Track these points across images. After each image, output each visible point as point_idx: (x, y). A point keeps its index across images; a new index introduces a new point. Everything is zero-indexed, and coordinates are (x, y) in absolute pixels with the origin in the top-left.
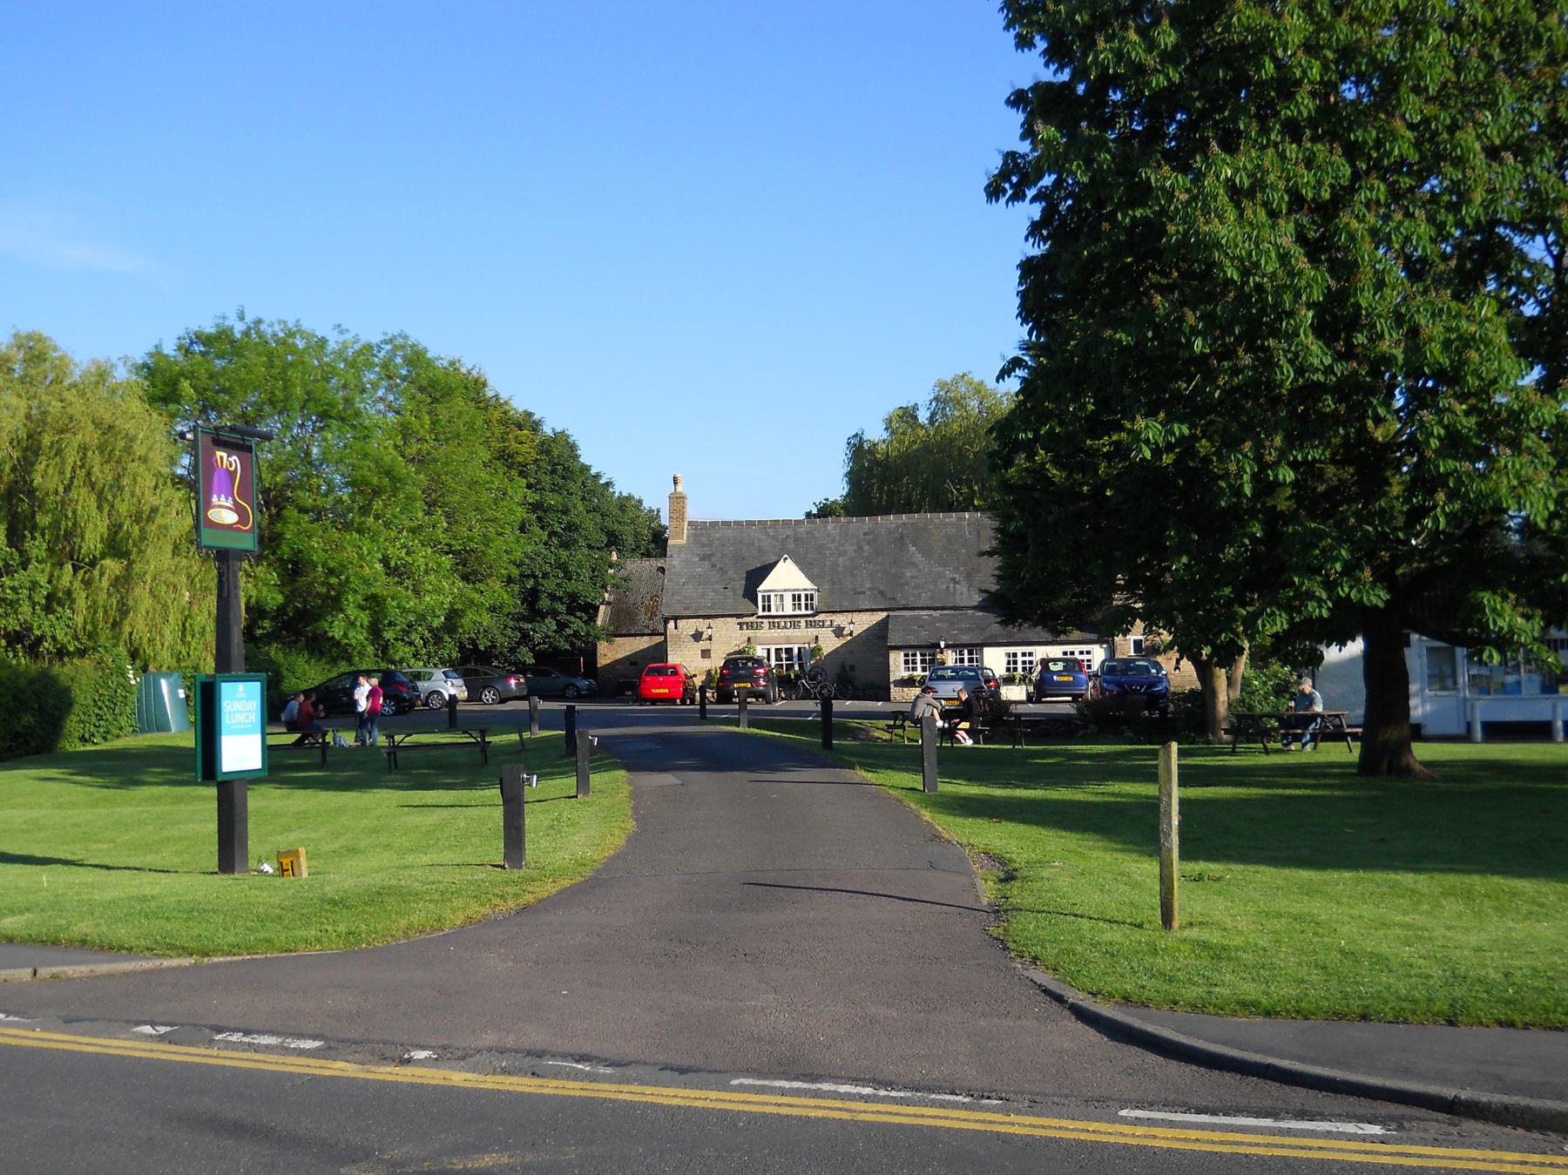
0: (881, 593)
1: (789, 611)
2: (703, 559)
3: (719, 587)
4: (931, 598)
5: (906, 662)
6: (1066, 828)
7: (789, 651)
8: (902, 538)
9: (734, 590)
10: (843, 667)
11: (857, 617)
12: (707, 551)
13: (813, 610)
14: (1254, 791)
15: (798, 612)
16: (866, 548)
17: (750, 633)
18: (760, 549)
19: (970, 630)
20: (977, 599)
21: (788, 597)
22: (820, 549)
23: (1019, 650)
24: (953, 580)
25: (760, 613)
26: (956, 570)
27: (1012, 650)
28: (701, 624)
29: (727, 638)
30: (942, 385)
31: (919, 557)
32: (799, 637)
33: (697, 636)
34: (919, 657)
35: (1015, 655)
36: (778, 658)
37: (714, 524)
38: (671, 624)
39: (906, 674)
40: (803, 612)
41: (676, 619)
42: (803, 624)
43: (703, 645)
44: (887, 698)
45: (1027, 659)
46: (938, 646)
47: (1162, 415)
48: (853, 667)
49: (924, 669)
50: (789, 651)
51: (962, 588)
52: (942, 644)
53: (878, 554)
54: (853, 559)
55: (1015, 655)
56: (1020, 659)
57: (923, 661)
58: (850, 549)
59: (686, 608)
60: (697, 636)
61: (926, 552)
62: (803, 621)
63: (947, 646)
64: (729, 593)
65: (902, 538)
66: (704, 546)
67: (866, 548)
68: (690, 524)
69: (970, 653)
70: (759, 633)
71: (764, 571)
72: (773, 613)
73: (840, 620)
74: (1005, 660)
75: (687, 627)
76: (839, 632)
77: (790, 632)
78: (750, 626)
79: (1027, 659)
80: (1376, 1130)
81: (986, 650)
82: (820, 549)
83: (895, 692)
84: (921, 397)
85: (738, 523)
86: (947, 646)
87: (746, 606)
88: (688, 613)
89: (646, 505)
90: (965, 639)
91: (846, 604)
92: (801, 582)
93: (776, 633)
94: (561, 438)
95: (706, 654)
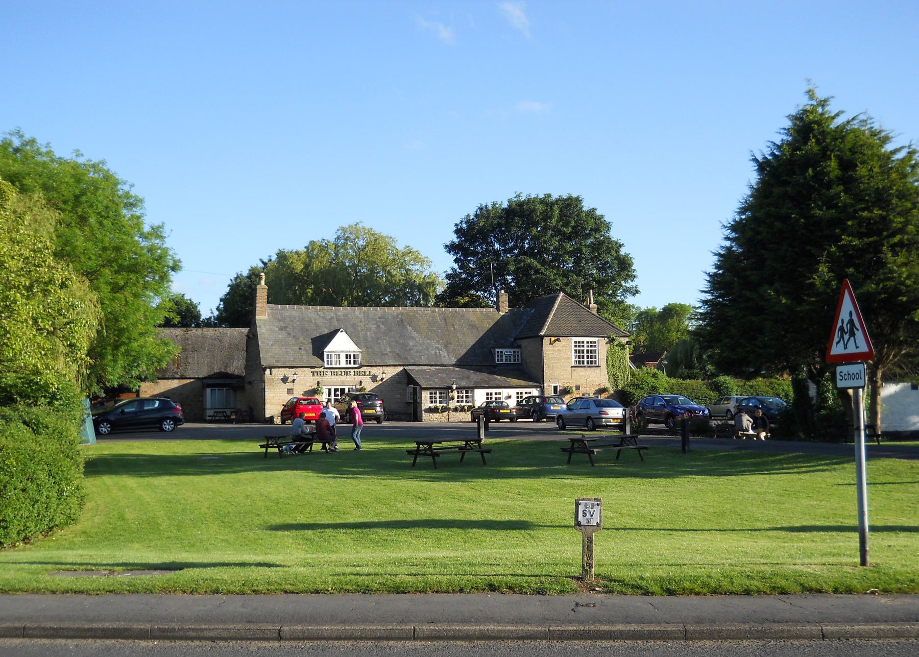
0: (398, 354)
1: (343, 364)
2: (281, 329)
3: (296, 348)
4: (428, 358)
5: (431, 398)
8: (402, 322)
9: (306, 350)
11: (386, 369)
12: (282, 324)
13: (354, 364)
14: (507, 469)
15: (349, 366)
16: (382, 326)
17: (319, 378)
20: (453, 361)
21: (343, 356)
23: (493, 391)
24: (437, 348)
25: (326, 366)
26: (438, 342)
27: (489, 391)
28: (289, 373)
29: (304, 381)
30: (344, 230)
31: (414, 334)
33: (285, 380)
34: (438, 395)
35: (491, 394)
40: (352, 365)
41: (271, 368)
42: (352, 373)
43: (289, 385)
44: (416, 417)
45: (498, 396)
46: (451, 388)
49: (441, 402)
51: (444, 353)
52: (454, 387)
53: (390, 331)
54: (376, 333)
55: (491, 394)
56: (494, 396)
57: (440, 397)
58: (373, 327)
59: (277, 361)
60: (285, 380)
61: (419, 331)
62: (352, 371)
64: (303, 352)
67: (382, 326)
69: (467, 392)
70: (325, 378)
72: (334, 366)
73: (375, 371)
74: (485, 396)
75: (279, 373)
76: (374, 378)
77: (344, 378)
78: (319, 374)
79: (498, 396)
81: (476, 391)
83: (425, 416)
84: (328, 234)
87: (315, 361)
88: (279, 364)
90: (463, 384)
91: (379, 362)
93: (335, 378)
95: (290, 391)
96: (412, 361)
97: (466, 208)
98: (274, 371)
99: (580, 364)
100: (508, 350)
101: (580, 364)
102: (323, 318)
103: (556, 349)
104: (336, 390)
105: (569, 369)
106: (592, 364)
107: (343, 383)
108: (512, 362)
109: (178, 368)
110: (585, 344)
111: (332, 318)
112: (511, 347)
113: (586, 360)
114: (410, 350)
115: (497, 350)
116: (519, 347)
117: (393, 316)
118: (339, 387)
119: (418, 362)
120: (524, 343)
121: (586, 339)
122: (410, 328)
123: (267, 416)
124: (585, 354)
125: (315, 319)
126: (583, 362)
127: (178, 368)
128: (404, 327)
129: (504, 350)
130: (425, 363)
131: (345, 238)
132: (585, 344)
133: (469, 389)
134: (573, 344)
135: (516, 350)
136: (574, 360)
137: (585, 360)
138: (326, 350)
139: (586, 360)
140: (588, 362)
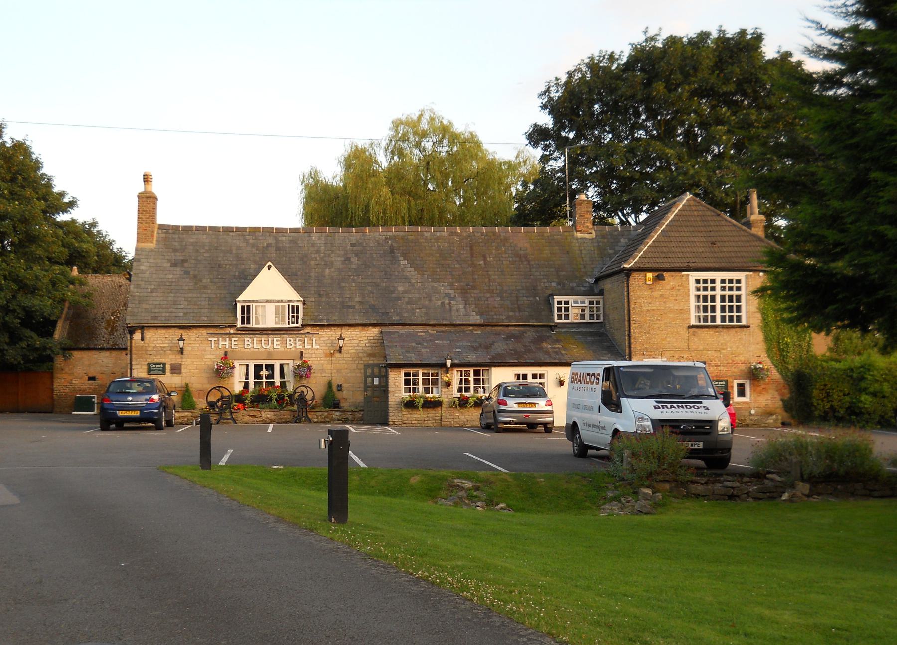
2: (174, 265)
4: (426, 313)
5: (407, 382)
6: (201, 438)
7: (270, 367)
10: (330, 384)
11: (347, 333)
12: (179, 256)
18: (239, 258)
19: (475, 349)
22: (304, 259)
23: (529, 371)
24: (447, 295)
26: (451, 285)
27: (522, 370)
31: (410, 271)
32: (283, 352)
36: (257, 376)
37: (188, 229)
38: (137, 336)
39: (406, 396)
41: (142, 328)
47: (870, 25)
48: (340, 388)
50: (270, 367)
51: (458, 304)
54: (340, 271)
58: (338, 261)
59: (155, 318)
61: (419, 268)
63: (454, 365)
65: (392, 251)
66: (175, 250)
67: (354, 259)
68: (161, 227)
71: (245, 279)
80: (120, 413)
82: (304, 259)
85: (212, 229)
86: (454, 365)
88: (156, 323)
89: (115, 247)
90: (472, 357)
91: (335, 318)
92: (288, 293)
94: (21, 147)
96: (395, 318)
97: (565, 59)
98: (149, 334)
99: (706, 325)
100: (579, 298)
101: (706, 325)
102: (253, 245)
103: (656, 294)
104: (258, 368)
105: (684, 333)
106: (732, 323)
107: (270, 355)
108: (587, 319)
109: (111, 333)
110: (718, 285)
111: (269, 245)
112: (589, 292)
113: (720, 316)
114: (399, 298)
115: (557, 298)
116: (601, 293)
117: (378, 242)
118: (264, 363)
119: (407, 317)
120: (607, 285)
121: (718, 276)
122: (404, 262)
123: (624, 401)
124: (718, 304)
125: (238, 248)
126: (713, 319)
127: (111, 333)
128: (394, 260)
129: (571, 299)
130: (419, 321)
131: (407, 132)
132: (718, 285)
133: (481, 368)
134: (692, 285)
135: (594, 298)
136: (693, 313)
137: (718, 314)
138: (241, 298)
139: (720, 316)
140: (723, 319)
